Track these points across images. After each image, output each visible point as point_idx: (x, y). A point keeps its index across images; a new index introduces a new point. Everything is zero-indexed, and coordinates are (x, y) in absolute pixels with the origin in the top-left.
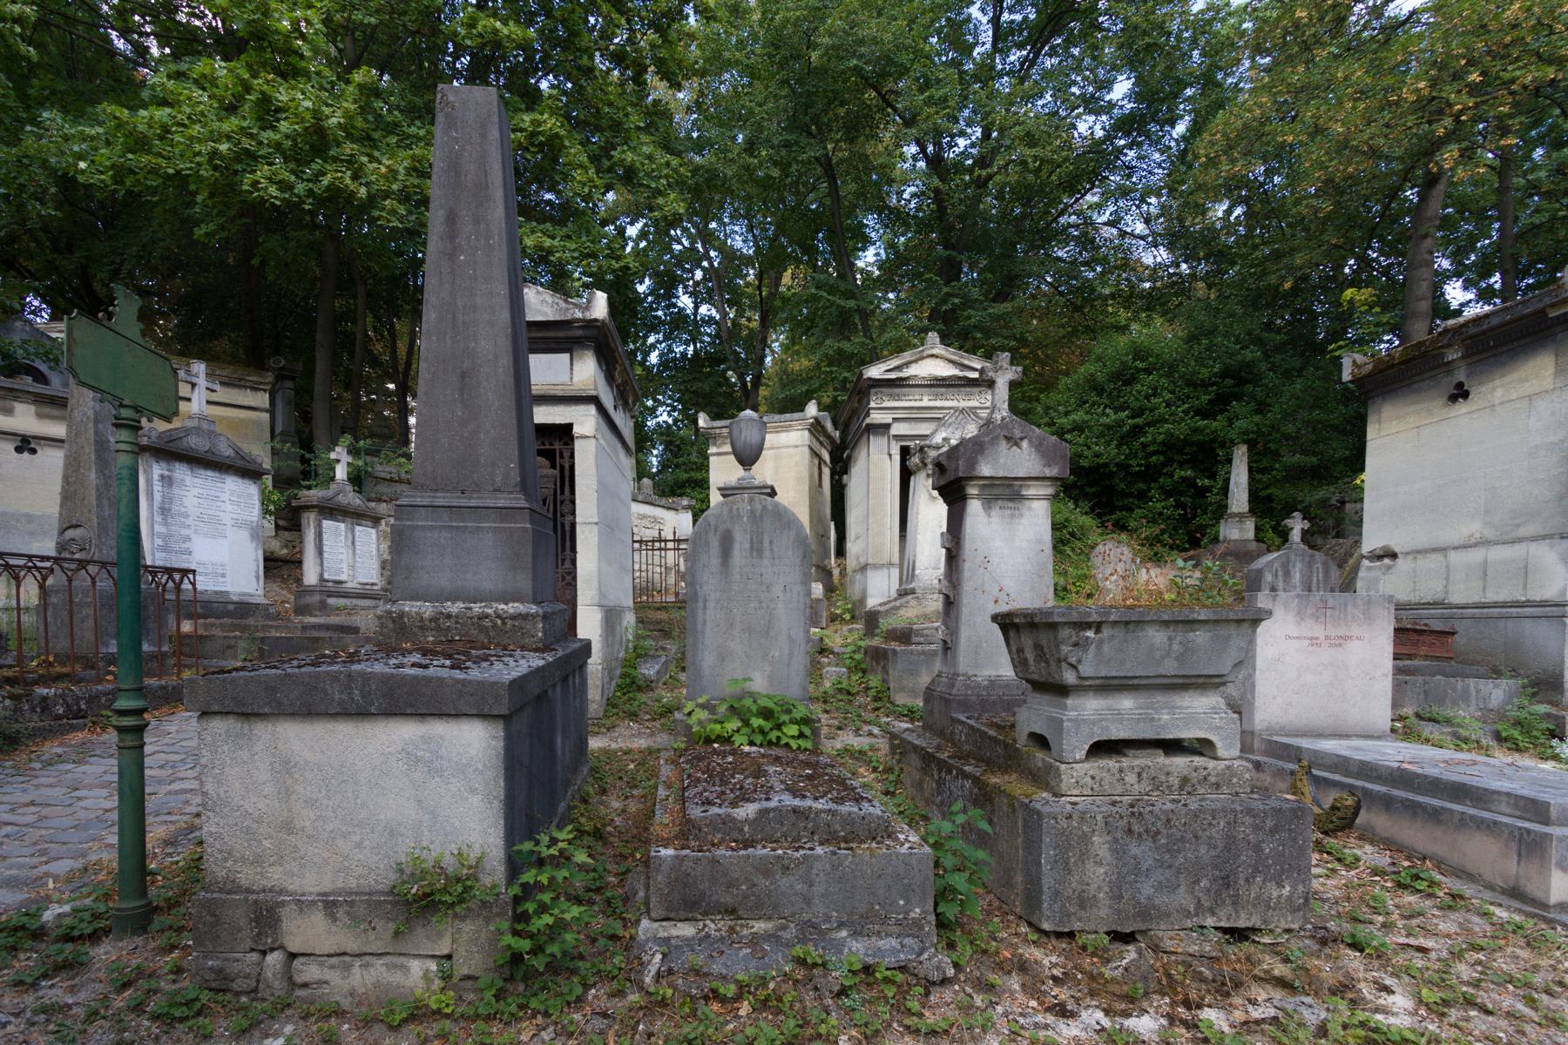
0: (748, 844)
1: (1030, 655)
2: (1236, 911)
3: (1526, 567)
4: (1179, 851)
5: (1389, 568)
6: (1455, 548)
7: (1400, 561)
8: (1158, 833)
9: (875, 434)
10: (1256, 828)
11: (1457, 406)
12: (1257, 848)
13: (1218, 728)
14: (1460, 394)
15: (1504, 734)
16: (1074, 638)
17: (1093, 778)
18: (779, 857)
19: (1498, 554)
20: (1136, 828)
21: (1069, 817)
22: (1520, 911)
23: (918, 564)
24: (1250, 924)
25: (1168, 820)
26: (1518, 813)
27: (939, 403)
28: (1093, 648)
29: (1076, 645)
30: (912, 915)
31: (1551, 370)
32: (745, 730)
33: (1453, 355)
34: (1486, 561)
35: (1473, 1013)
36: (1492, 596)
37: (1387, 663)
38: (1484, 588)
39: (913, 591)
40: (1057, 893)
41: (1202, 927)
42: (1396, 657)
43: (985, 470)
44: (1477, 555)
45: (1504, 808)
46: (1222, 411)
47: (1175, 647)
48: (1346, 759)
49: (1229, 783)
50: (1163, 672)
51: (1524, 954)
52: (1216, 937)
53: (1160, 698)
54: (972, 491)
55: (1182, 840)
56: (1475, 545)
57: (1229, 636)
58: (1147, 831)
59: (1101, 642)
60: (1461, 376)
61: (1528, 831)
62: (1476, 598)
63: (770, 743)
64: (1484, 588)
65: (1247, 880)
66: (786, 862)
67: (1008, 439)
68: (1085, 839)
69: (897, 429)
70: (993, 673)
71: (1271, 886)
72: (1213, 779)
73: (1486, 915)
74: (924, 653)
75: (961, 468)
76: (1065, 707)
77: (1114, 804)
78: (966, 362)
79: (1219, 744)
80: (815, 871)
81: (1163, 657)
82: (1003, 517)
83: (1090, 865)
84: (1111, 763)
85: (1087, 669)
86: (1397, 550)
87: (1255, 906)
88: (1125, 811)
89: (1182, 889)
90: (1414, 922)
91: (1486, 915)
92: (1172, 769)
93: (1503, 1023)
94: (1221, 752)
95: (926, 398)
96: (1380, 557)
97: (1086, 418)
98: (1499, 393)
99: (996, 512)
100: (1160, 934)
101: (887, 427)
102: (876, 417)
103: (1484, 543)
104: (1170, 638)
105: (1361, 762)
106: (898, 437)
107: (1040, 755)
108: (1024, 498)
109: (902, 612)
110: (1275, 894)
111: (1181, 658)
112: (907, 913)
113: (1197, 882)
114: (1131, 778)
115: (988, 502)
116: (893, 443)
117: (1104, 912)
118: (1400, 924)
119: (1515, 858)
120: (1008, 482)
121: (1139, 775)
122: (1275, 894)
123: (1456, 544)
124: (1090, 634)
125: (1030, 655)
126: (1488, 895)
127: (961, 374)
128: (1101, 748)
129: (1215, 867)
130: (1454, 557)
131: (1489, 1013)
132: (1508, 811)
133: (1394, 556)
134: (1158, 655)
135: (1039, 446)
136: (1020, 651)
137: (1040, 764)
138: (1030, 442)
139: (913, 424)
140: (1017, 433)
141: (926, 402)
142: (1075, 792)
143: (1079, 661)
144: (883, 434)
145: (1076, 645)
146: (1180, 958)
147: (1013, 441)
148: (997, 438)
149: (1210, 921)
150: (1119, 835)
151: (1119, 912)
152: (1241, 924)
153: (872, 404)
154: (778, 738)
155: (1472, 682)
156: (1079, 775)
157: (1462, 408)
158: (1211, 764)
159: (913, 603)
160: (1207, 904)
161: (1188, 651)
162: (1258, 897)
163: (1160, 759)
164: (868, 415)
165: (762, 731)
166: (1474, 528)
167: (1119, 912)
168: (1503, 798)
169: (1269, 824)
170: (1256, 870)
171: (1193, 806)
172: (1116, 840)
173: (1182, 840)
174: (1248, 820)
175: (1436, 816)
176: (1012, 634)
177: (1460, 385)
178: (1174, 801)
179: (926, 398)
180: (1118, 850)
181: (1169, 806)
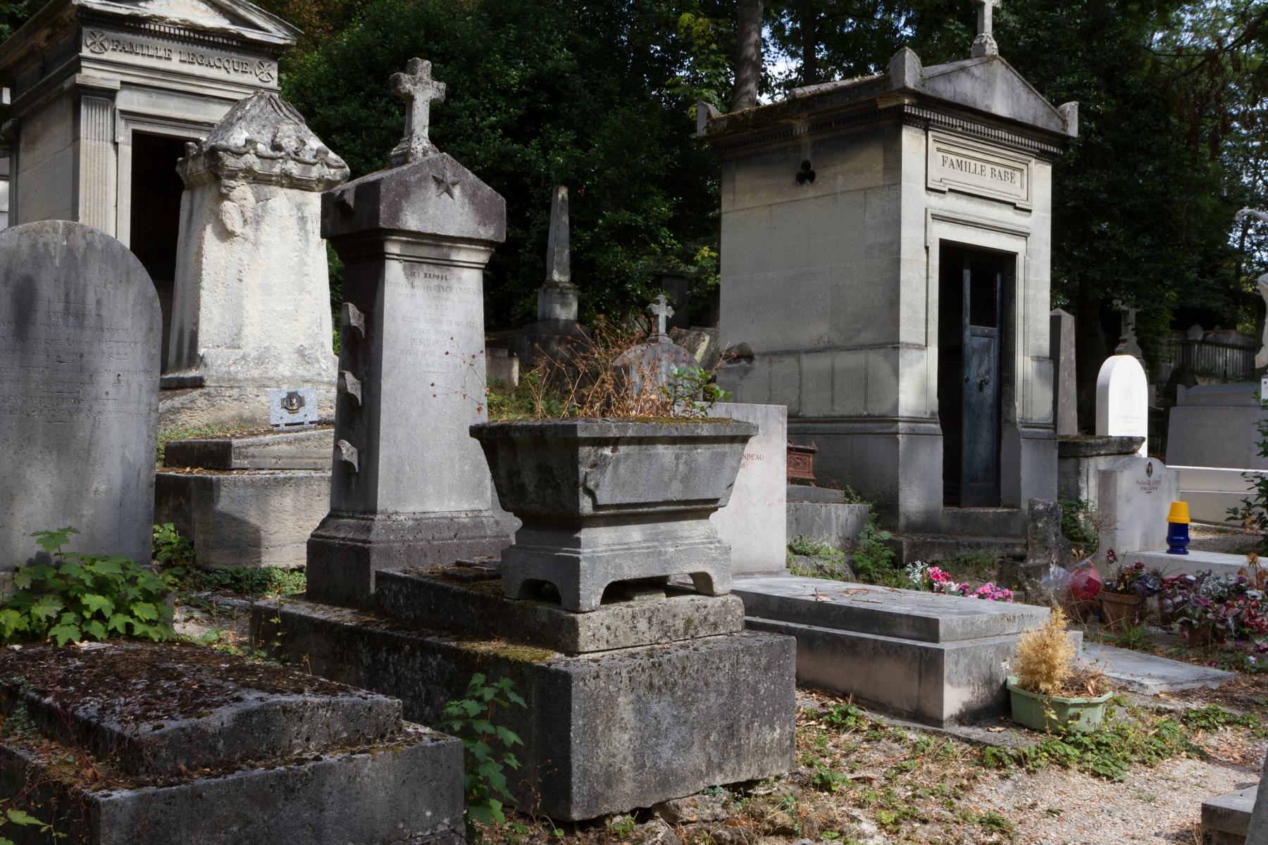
0: (228, 767)
1: (529, 480)
2: (739, 763)
3: (866, 378)
4: (692, 703)
5: (747, 371)
6: (807, 352)
7: (756, 363)
8: (675, 684)
9: (91, 104)
10: (754, 667)
11: (805, 187)
12: (755, 691)
13: (714, 559)
14: (806, 176)
15: (860, 565)
16: (592, 458)
17: (608, 628)
18: (281, 776)
19: (846, 361)
20: (657, 681)
21: (597, 677)
22: (924, 731)
23: (202, 338)
24: (749, 777)
25: (684, 668)
26: (915, 634)
27: (196, 70)
28: (610, 468)
29: (594, 465)
30: (441, 828)
31: (880, 167)
32: (70, 617)
33: (800, 127)
34: (833, 369)
35: (916, 825)
36: (840, 410)
37: (782, 486)
38: (832, 400)
39: (198, 383)
40: (585, 772)
41: (713, 787)
42: (791, 480)
43: (412, 222)
44: (824, 362)
45: (905, 631)
46: (535, 134)
47: (681, 467)
48: (766, 598)
49: (725, 622)
50: (670, 496)
51: (933, 767)
52: (724, 795)
53: (663, 527)
54: (393, 248)
55: (695, 690)
56: (823, 350)
57: (724, 454)
58: (665, 684)
59: (618, 461)
60: (807, 155)
61: (926, 649)
62: (825, 411)
63: (113, 634)
64: (832, 400)
65: (747, 728)
66: (290, 782)
67: (439, 182)
68: (611, 700)
69: (126, 101)
70: (419, 509)
71: (766, 729)
72: (711, 619)
73: (899, 740)
74: (253, 484)
75: (383, 216)
76: (577, 543)
77: (633, 656)
78: (241, 12)
79: (715, 579)
80: (327, 789)
81: (671, 480)
82: (428, 288)
83: (616, 733)
84: (620, 608)
85: (604, 497)
86: (754, 349)
87: (753, 756)
88: (646, 663)
89: (695, 748)
90: (853, 757)
91: (899, 740)
92: (677, 610)
93: (938, 828)
94: (718, 588)
95: (176, 57)
96: (738, 358)
97: (363, 113)
98: (840, 179)
99: (419, 281)
100: (679, 802)
101: (111, 94)
102: (91, 75)
103: (830, 348)
104: (677, 457)
105: (781, 599)
106: (129, 115)
107: (543, 608)
108: (452, 264)
109: (184, 417)
110: (769, 738)
111: (685, 480)
112: (434, 827)
113: (707, 737)
114: (642, 625)
115: (412, 263)
116: (121, 124)
117: (628, 786)
118: (843, 761)
119: (917, 679)
120: (437, 240)
121: (650, 619)
122: (769, 738)
123: (808, 347)
124: (607, 451)
125: (529, 480)
126: (898, 722)
127: (234, 29)
128: (618, 592)
129: (722, 717)
130: (807, 361)
131: (925, 822)
132: (908, 633)
133: (750, 357)
134: (666, 477)
135: (472, 197)
136: (514, 474)
137: (544, 619)
138: (463, 189)
139: (155, 97)
140: (449, 177)
141: (175, 64)
142: (592, 648)
143: (597, 486)
144: (104, 107)
145: (594, 465)
146: (697, 826)
147: (444, 186)
148: (424, 179)
149: (719, 780)
150: (642, 691)
151: (642, 783)
152: (743, 777)
153: (85, 52)
154: (129, 627)
155: (832, 506)
156: (597, 623)
157: (809, 191)
158: (710, 601)
159: (201, 402)
160: (716, 760)
161: (692, 471)
162: (756, 745)
163: (660, 599)
164: (79, 69)
165: (99, 616)
166: (819, 330)
167: (642, 783)
168: (905, 621)
169: (764, 661)
170: (755, 715)
171: (703, 650)
172: (639, 698)
173: (695, 690)
174: (747, 659)
175: (853, 646)
176: (502, 453)
177: (806, 165)
178: (682, 647)
179: (176, 57)
180: (641, 710)
181: (682, 652)
